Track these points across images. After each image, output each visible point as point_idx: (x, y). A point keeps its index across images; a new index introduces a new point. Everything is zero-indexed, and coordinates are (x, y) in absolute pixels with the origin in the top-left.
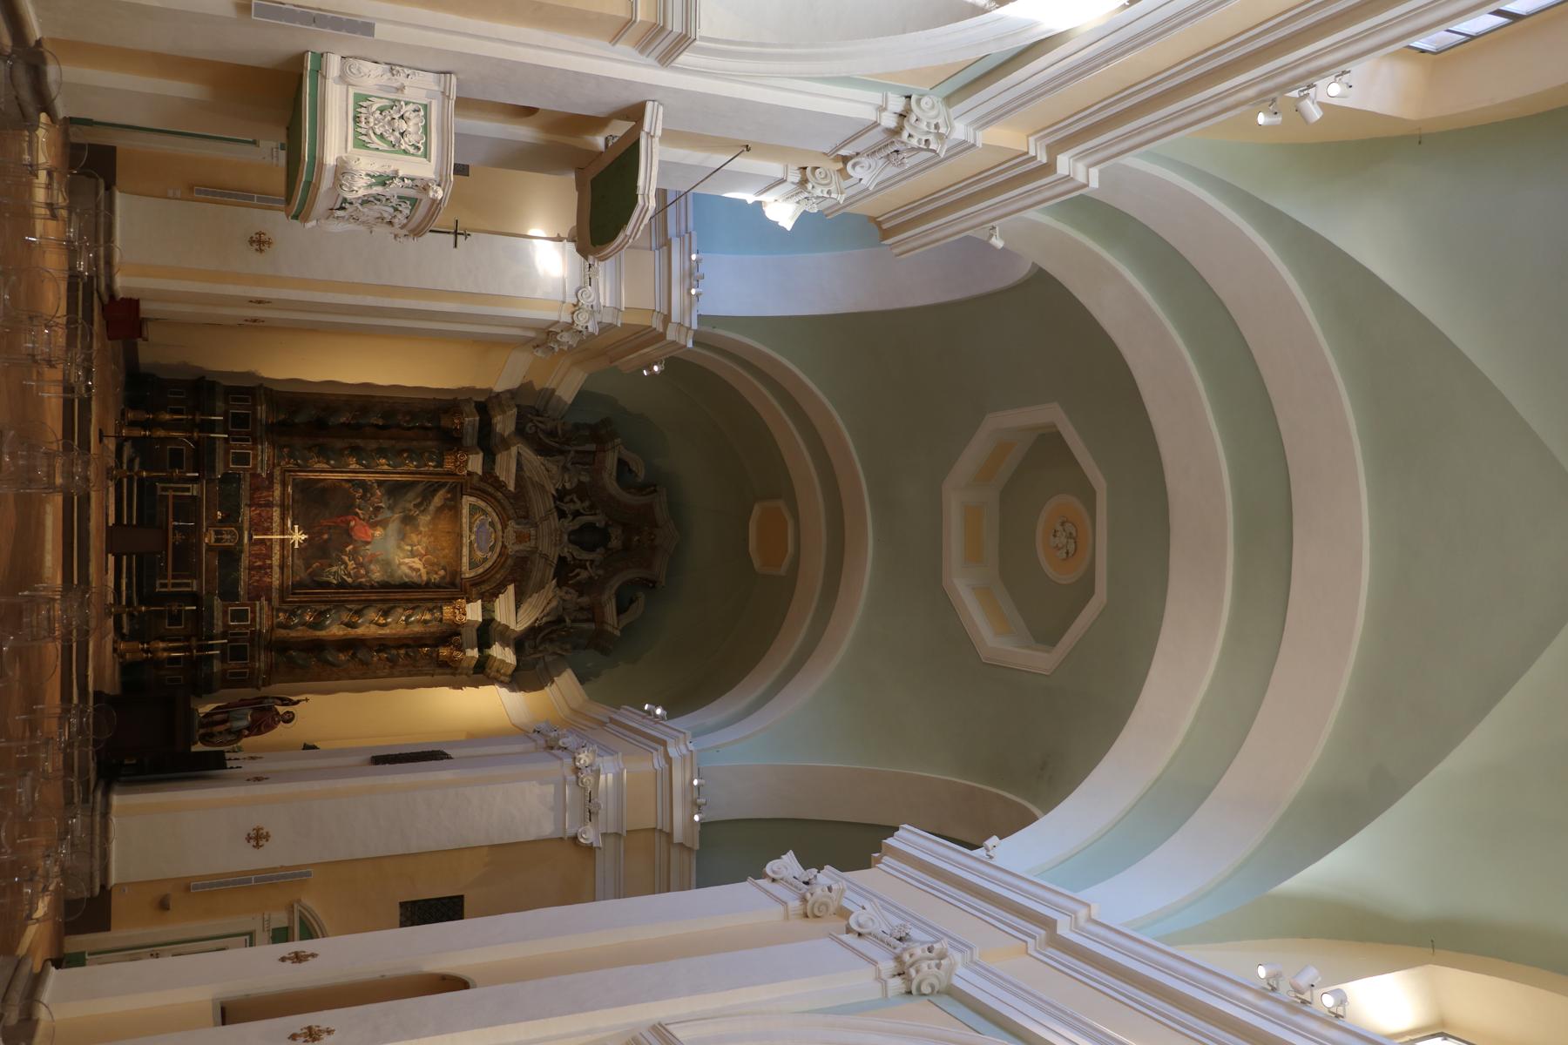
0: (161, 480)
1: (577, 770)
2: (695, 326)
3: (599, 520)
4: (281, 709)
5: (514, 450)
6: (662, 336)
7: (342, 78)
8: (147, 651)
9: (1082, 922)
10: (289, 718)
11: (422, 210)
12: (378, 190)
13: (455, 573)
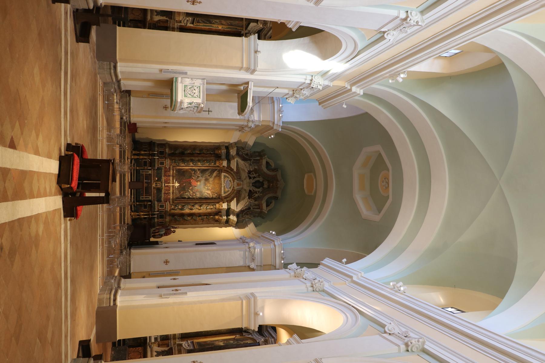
0: (142, 169)
1: (249, 248)
2: (281, 125)
3: (261, 179)
4: (172, 229)
5: (236, 159)
6: (272, 128)
7: (181, 82)
8: (138, 215)
9: (359, 277)
10: (174, 232)
11: (199, 109)
12: (189, 105)
13: (220, 195)
